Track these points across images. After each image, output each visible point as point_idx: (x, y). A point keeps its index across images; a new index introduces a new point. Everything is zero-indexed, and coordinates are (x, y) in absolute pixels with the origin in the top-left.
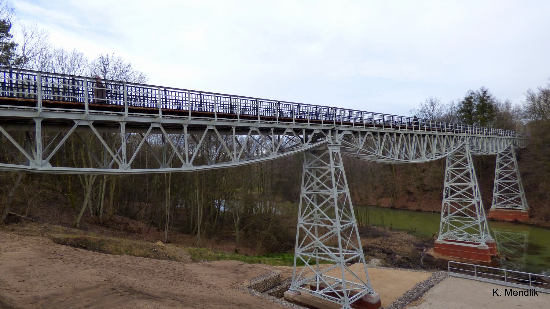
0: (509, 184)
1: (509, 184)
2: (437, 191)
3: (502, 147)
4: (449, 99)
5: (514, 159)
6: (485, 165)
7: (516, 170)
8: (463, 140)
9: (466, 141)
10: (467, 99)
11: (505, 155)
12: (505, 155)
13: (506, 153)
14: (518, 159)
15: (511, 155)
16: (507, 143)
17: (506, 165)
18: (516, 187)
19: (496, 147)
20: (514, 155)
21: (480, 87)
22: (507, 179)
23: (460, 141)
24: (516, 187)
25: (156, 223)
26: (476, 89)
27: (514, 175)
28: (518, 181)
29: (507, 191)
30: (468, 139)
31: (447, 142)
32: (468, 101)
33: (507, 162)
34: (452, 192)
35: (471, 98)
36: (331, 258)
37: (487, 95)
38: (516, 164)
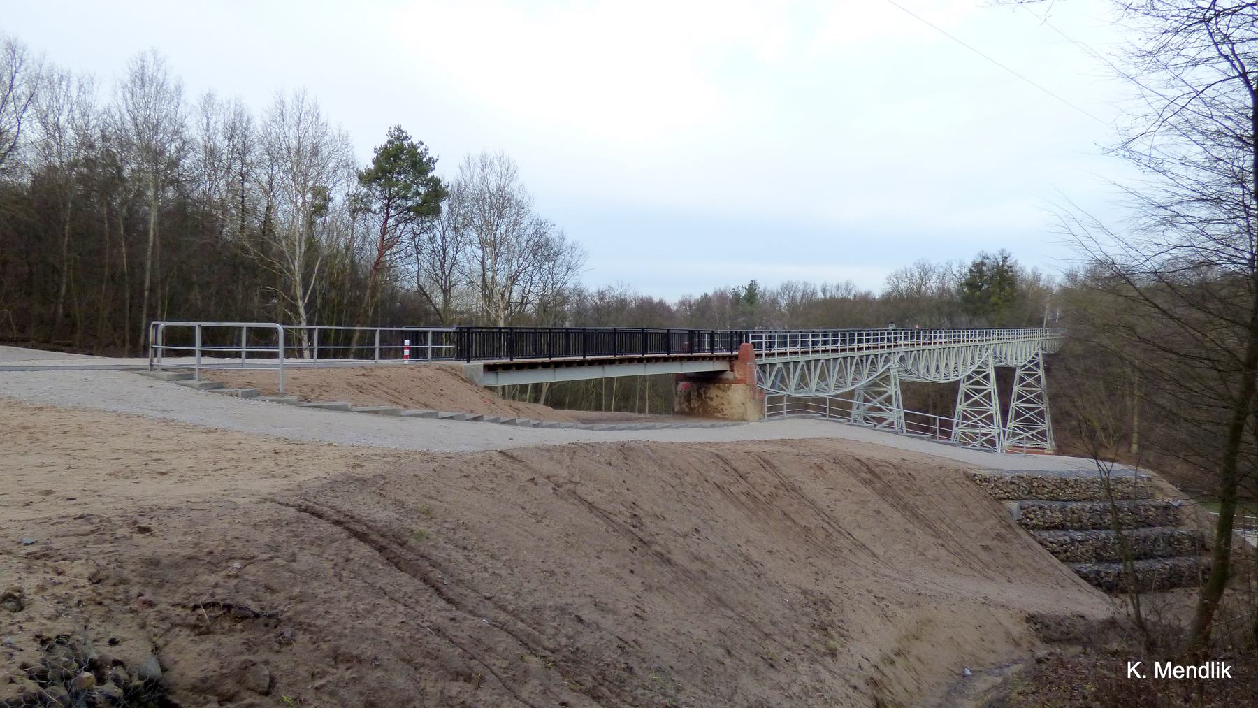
0: (1030, 409)
1: (1030, 409)
2: (949, 409)
3: (960, 368)
4: (949, 259)
5: (1041, 372)
6: (1005, 376)
7: (1042, 388)
8: (887, 361)
9: (894, 362)
10: (975, 265)
11: (977, 378)
12: (977, 378)
13: (978, 373)
14: (1047, 370)
15: (1037, 365)
16: (964, 365)
17: (1029, 380)
18: (1041, 414)
19: (937, 367)
20: (1042, 365)
21: (999, 248)
22: (1028, 401)
23: (881, 362)
24: (1041, 414)
25: (987, 480)
26: (993, 251)
27: (1039, 397)
28: (1044, 406)
29: (1027, 420)
30: (898, 357)
31: (840, 370)
32: (978, 268)
33: (1030, 376)
34: (965, 418)
35: (982, 264)
36: (519, 392)
37: (1008, 264)
38: (1043, 381)
